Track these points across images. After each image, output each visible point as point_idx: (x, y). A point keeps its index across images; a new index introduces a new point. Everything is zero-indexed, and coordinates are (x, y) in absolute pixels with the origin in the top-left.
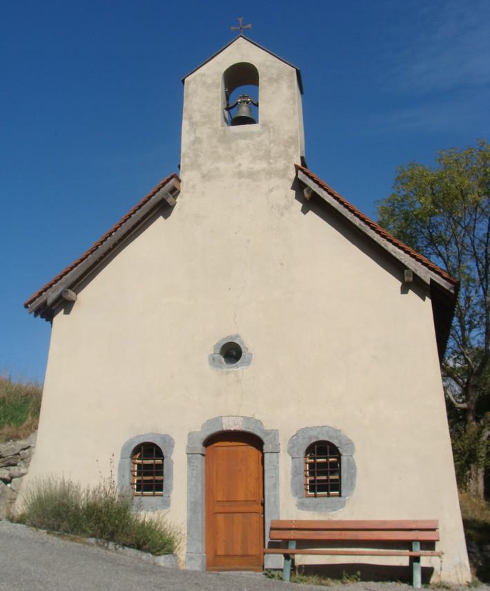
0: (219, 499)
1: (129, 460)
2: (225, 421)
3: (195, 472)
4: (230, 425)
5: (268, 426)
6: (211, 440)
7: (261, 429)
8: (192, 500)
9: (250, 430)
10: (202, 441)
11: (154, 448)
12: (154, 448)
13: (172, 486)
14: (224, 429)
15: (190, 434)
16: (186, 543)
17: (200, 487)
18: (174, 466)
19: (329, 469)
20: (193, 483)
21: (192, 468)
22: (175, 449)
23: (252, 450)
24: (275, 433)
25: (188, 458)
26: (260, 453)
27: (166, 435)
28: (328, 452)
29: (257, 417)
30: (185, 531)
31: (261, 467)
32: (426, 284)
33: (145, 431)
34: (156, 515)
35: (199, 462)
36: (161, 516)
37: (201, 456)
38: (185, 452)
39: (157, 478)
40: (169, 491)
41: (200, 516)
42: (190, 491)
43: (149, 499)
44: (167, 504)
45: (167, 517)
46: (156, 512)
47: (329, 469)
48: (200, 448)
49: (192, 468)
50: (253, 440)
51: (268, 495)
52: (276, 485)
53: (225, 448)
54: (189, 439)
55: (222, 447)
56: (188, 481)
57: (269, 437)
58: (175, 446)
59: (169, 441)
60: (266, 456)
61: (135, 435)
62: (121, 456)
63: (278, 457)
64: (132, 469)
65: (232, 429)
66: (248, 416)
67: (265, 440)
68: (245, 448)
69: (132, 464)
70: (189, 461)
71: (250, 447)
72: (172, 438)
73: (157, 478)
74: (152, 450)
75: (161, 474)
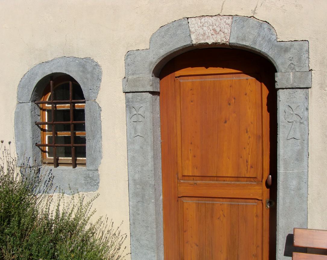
0: (186, 174)
1: (28, 106)
2: (194, 25)
3: (139, 127)
4: (204, 34)
5: (284, 34)
6: (169, 66)
7: (270, 40)
8: (137, 176)
9: (247, 43)
10: (153, 67)
11: (71, 83)
12: (71, 83)
13: (100, 152)
14: (194, 42)
15: (128, 54)
16: (128, 250)
17: (150, 154)
18: (104, 116)
19: (70, 122)
20: (137, 147)
21: (134, 119)
22: (103, 84)
23: (250, 86)
24: (301, 46)
25: (128, 101)
26: (265, 88)
27: (88, 59)
28: (68, 122)
29: (261, 15)
30: (126, 229)
31: (266, 115)
32: (59, 131)
33: (52, 53)
34: (76, 201)
35: (149, 107)
36: (84, 203)
37: (150, 95)
38: (120, 89)
39: (83, 145)
40: (96, 160)
41: (152, 207)
42: (132, 162)
43: (65, 173)
44: (93, 182)
45: (95, 205)
46: (76, 195)
47: (70, 122)
48: (148, 81)
49: (134, 119)
50: (258, 66)
51: (285, 174)
52: (301, 156)
53: (198, 80)
54: (127, 65)
55: (190, 77)
56: (129, 143)
57: (289, 55)
58: (104, 78)
59: (91, 67)
60: (282, 96)
61: (37, 62)
62: (18, 98)
63: (307, 98)
64: (39, 120)
65: (210, 41)
66: (240, 13)
67: (279, 62)
68: (235, 78)
69: (38, 111)
70: (129, 106)
71: (245, 77)
72: (97, 65)
73: (83, 145)
74: (67, 87)
75: (82, 127)
